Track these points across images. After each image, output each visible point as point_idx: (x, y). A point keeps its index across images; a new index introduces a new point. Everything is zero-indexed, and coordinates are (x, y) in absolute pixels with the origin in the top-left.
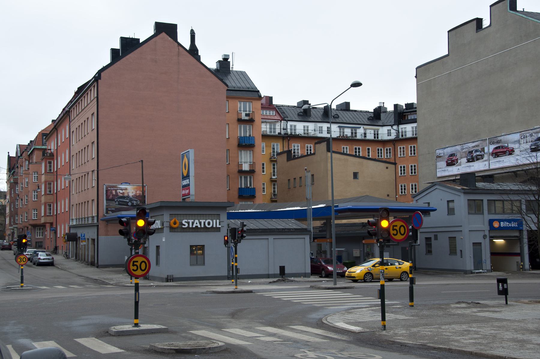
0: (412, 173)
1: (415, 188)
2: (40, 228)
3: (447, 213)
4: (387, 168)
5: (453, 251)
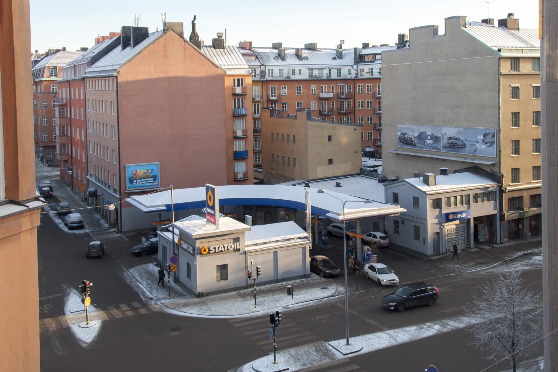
0: (368, 107)
1: (371, 120)
2: (50, 149)
3: (413, 206)
4: (355, 130)
5: (417, 236)
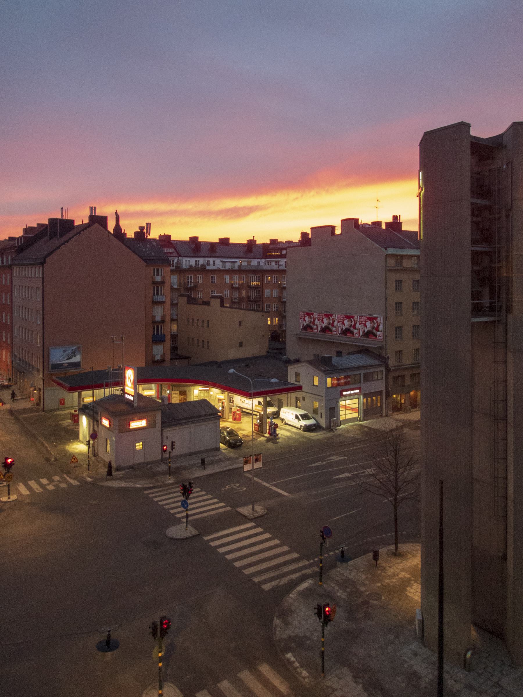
4: (263, 316)
